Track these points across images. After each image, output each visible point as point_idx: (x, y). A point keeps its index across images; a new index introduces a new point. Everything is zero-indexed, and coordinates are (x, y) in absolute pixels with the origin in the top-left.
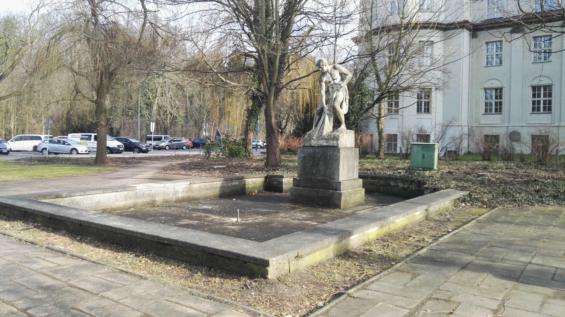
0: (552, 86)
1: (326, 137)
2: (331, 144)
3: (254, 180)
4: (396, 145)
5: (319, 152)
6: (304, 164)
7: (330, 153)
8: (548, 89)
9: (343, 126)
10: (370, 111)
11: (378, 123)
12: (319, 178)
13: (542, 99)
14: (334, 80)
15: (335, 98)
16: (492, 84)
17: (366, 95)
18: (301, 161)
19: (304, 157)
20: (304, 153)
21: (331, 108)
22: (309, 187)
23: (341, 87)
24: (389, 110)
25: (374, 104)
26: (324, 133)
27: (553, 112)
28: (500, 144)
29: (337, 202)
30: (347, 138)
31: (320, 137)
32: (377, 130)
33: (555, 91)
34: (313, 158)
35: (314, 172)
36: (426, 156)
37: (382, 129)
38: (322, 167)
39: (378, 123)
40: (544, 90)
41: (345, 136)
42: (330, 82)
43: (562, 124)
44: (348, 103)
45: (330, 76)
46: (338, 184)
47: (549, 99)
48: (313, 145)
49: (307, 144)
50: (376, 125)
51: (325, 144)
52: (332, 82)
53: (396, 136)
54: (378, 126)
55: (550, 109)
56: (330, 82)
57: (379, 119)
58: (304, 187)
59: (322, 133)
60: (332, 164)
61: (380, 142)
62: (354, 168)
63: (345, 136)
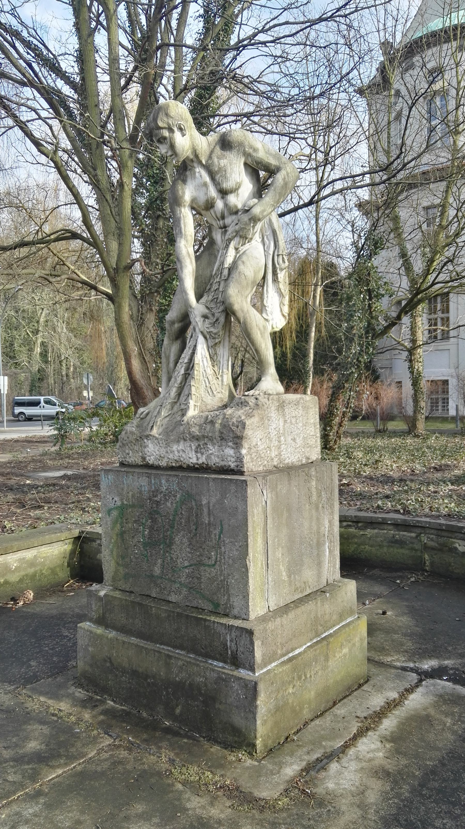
1: (195, 430)
2: (215, 461)
3: (29, 554)
4: (446, 401)
5: (168, 495)
6: (122, 534)
7: (210, 494)
9: (271, 382)
10: (393, 332)
11: (411, 361)
12: (173, 598)
14: (224, 193)
15: (231, 269)
17: (379, 296)
18: (115, 523)
19: (122, 509)
21: (218, 311)
22: (140, 635)
23: (255, 220)
24: (430, 332)
25: (399, 318)
26: (192, 412)
29: (238, 720)
30: (284, 429)
31: (177, 430)
32: (409, 375)
34: (153, 514)
35: (157, 571)
37: (419, 373)
38: (182, 552)
39: (411, 361)
41: (276, 422)
42: (210, 205)
44: (285, 288)
45: (207, 179)
46: (244, 640)
48: (151, 460)
49: (134, 458)
50: (407, 364)
51: (192, 458)
52: (220, 204)
53: (446, 382)
54: (411, 367)
56: (210, 205)
57: (411, 351)
58: (122, 630)
59: (184, 412)
61: (416, 400)
62: (319, 545)
63: (276, 422)
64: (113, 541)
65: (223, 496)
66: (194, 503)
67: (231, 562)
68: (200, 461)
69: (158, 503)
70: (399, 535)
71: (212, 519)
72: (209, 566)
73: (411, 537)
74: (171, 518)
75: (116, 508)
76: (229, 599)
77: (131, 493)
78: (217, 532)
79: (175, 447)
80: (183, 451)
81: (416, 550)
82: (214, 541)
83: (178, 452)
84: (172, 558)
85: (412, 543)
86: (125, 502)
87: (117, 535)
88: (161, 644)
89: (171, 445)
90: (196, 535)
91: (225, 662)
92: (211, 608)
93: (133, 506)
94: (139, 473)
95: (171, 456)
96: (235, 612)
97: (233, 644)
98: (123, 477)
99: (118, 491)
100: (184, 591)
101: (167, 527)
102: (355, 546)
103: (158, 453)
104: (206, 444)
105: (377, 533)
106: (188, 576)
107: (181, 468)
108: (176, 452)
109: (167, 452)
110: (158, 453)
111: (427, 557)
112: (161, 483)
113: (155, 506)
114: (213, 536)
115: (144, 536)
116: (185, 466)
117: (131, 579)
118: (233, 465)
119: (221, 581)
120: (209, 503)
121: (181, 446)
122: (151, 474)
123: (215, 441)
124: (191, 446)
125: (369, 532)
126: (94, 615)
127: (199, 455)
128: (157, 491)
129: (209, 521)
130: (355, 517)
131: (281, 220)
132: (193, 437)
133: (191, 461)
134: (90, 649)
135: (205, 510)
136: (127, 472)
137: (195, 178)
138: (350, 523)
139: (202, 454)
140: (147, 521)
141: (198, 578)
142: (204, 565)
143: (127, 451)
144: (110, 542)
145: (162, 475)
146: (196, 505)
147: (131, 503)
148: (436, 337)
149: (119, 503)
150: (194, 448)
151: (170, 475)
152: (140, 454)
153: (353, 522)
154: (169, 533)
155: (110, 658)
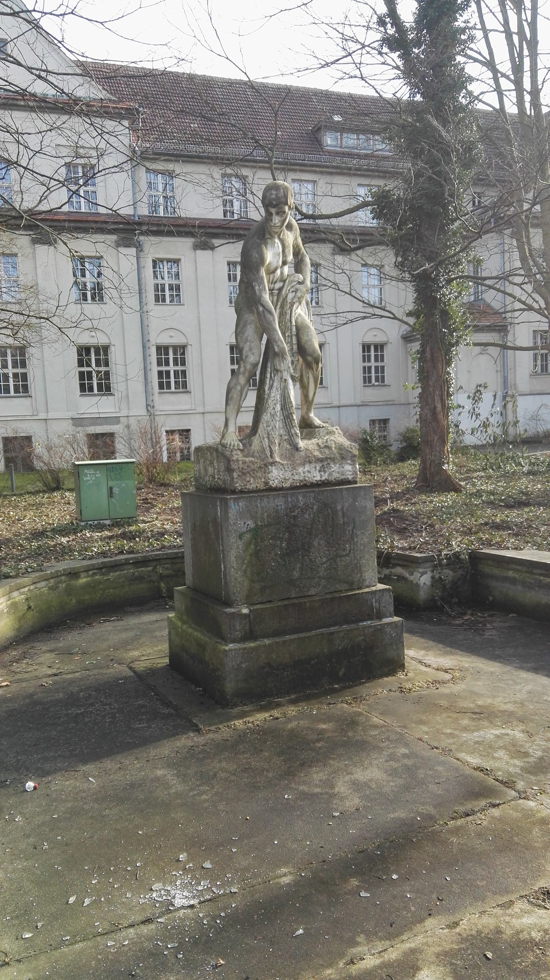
0: (186, 346)
6: (256, 554)
8: (181, 350)
12: (313, 592)
13: (373, 364)
16: (171, 337)
19: (256, 532)
20: (253, 518)
27: (33, 395)
28: (253, 447)
29: (391, 653)
33: (191, 356)
35: (296, 574)
36: (116, 490)
40: (175, 353)
43: (51, 415)
47: (23, 371)
48: (274, 483)
51: (317, 476)
55: (26, 388)
60: (353, 535)
64: (246, 562)
65: (355, 500)
66: (329, 511)
67: (362, 548)
68: (324, 478)
69: (295, 517)
70: (137, 571)
71: (346, 519)
72: (344, 556)
73: (149, 571)
74: (309, 527)
75: (251, 530)
76: (361, 576)
77: (266, 514)
78: (350, 528)
79: (301, 470)
80: (309, 472)
81: (154, 582)
82: (348, 536)
83: (304, 473)
84: (311, 560)
85: (150, 576)
86: (260, 524)
87: (251, 555)
88: (316, 630)
89: (297, 468)
90: (332, 535)
91: (372, 619)
92: (346, 586)
93: (269, 525)
94: (274, 495)
95: (296, 477)
96: (367, 583)
97: (377, 604)
98: (256, 501)
99: (251, 515)
100: (323, 582)
101: (305, 535)
102: (101, 592)
103: (282, 476)
104: (329, 464)
105: (118, 575)
106: (326, 570)
107: (305, 486)
108: (302, 474)
109: (293, 475)
110: (282, 476)
111: (162, 585)
112: (297, 499)
113: (292, 520)
114: (347, 532)
115: (281, 548)
116: (309, 484)
117: (268, 591)
118: (350, 478)
119: (355, 564)
120: (343, 507)
121: (307, 467)
122: (287, 494)
123: (336, 461)
124: (315, 467)
125: (112, 576)
126: (238, 634)
127: (322, 473)
128: (294, 507)
129: (344, 522)
130: (102, 563)
131: (15, 250)
132: (318, 459)
133: (315, 479)
134: (243, 666)
135: (340, 514)
136: (261, 496)
137: (274, 247)
138: (95, 571)
139: (325, 472)
140: (284, 534)
141: (335, 569)
142: (341, 556)
143: (248, 479)
144: (243, 563)
145: (299, 493)
146: (332, 511)
147: (266, 523)
148: (97, 353)
149: (252, 526)
150: (318, 468)
151: (307, 492)
152: (263, 480)
153: (97, 569)
154: (307, 540)
155: (269, 663)
